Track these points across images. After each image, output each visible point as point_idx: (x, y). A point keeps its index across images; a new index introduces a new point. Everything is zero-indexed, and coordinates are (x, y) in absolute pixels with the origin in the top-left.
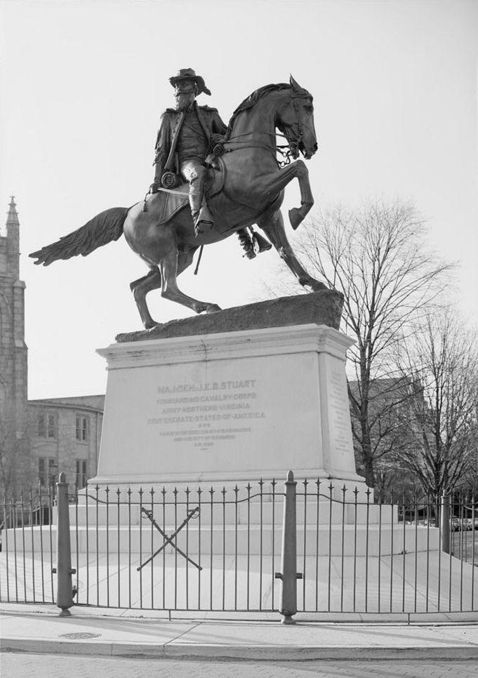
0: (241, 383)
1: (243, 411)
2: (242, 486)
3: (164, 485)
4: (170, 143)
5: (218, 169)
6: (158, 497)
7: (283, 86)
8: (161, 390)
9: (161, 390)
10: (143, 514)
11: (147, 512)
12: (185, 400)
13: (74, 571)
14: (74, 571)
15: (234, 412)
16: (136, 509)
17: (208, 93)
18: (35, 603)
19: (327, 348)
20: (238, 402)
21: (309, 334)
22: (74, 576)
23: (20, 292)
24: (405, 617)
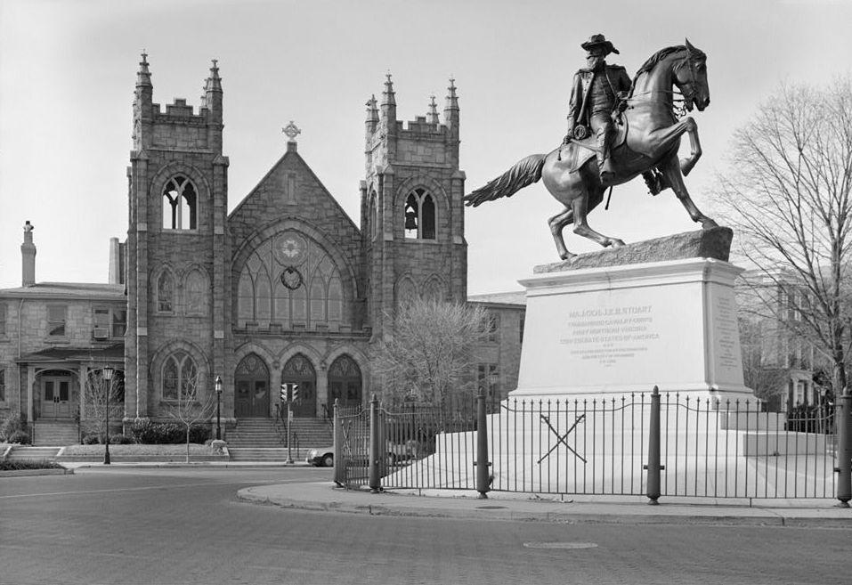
0: (639, 309)
1: (640, 333)
2: (618, 397)
3: (541, 397)
4: (582, 99)
5: (621, 123)
6: (554, 407)
7: (682, 49)
8: (572, 315)
9: (572, 315)
10: (542, 419)
11: (545, 418)
12: (592, 323)
13: (490, 464)
14: (490, 464)
15: (633, 334)
16: (536, 416)
17: (617, 52)
18: (460, 489)
19: (710, 280)
20: (636, 325)
21: (694, 267)
22: (490, 468)
23: (459, 212)
24: (747, 502)
